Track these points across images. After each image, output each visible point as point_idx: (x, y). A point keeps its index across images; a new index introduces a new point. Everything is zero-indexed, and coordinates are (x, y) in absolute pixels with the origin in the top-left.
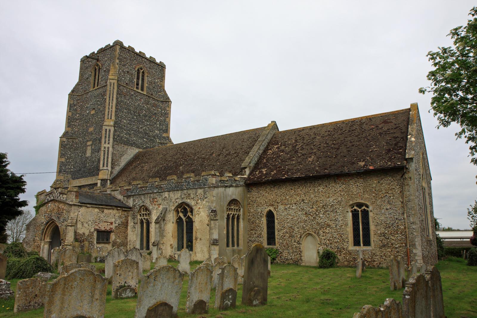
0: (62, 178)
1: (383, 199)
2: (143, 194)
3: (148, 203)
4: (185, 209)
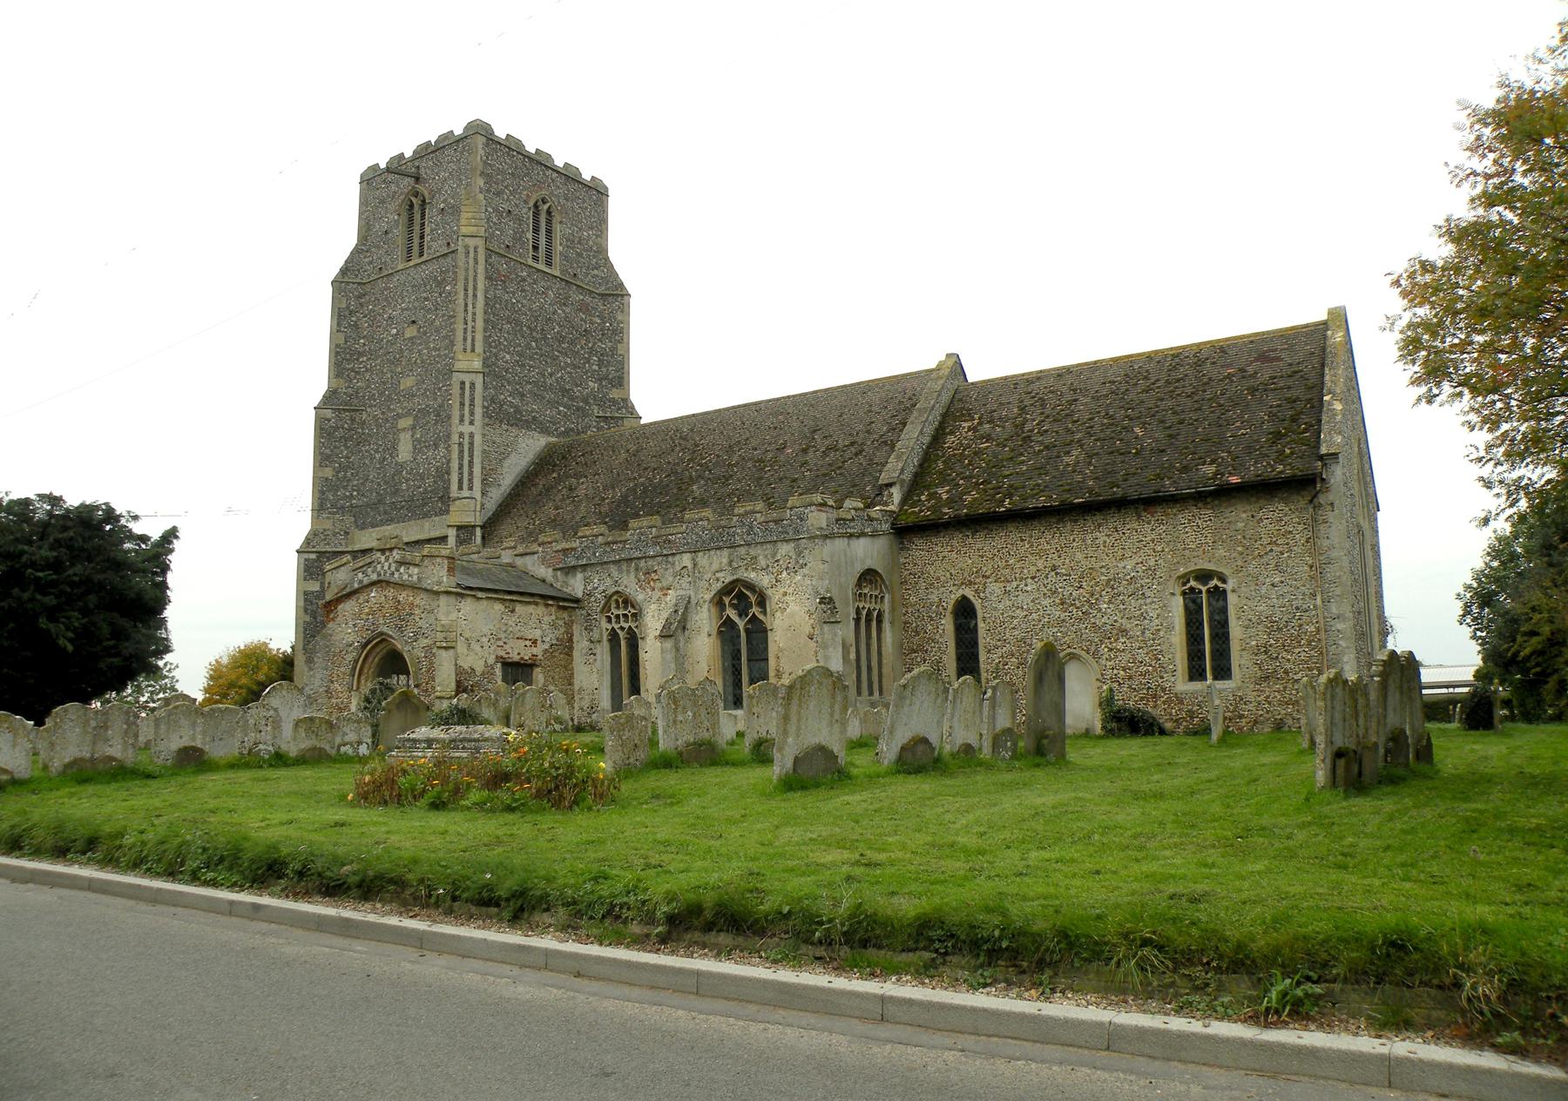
0: (328, 525)
1: (1265, 559)
2: (614, 562)
3: (629, 583)
4: (741, 597)
